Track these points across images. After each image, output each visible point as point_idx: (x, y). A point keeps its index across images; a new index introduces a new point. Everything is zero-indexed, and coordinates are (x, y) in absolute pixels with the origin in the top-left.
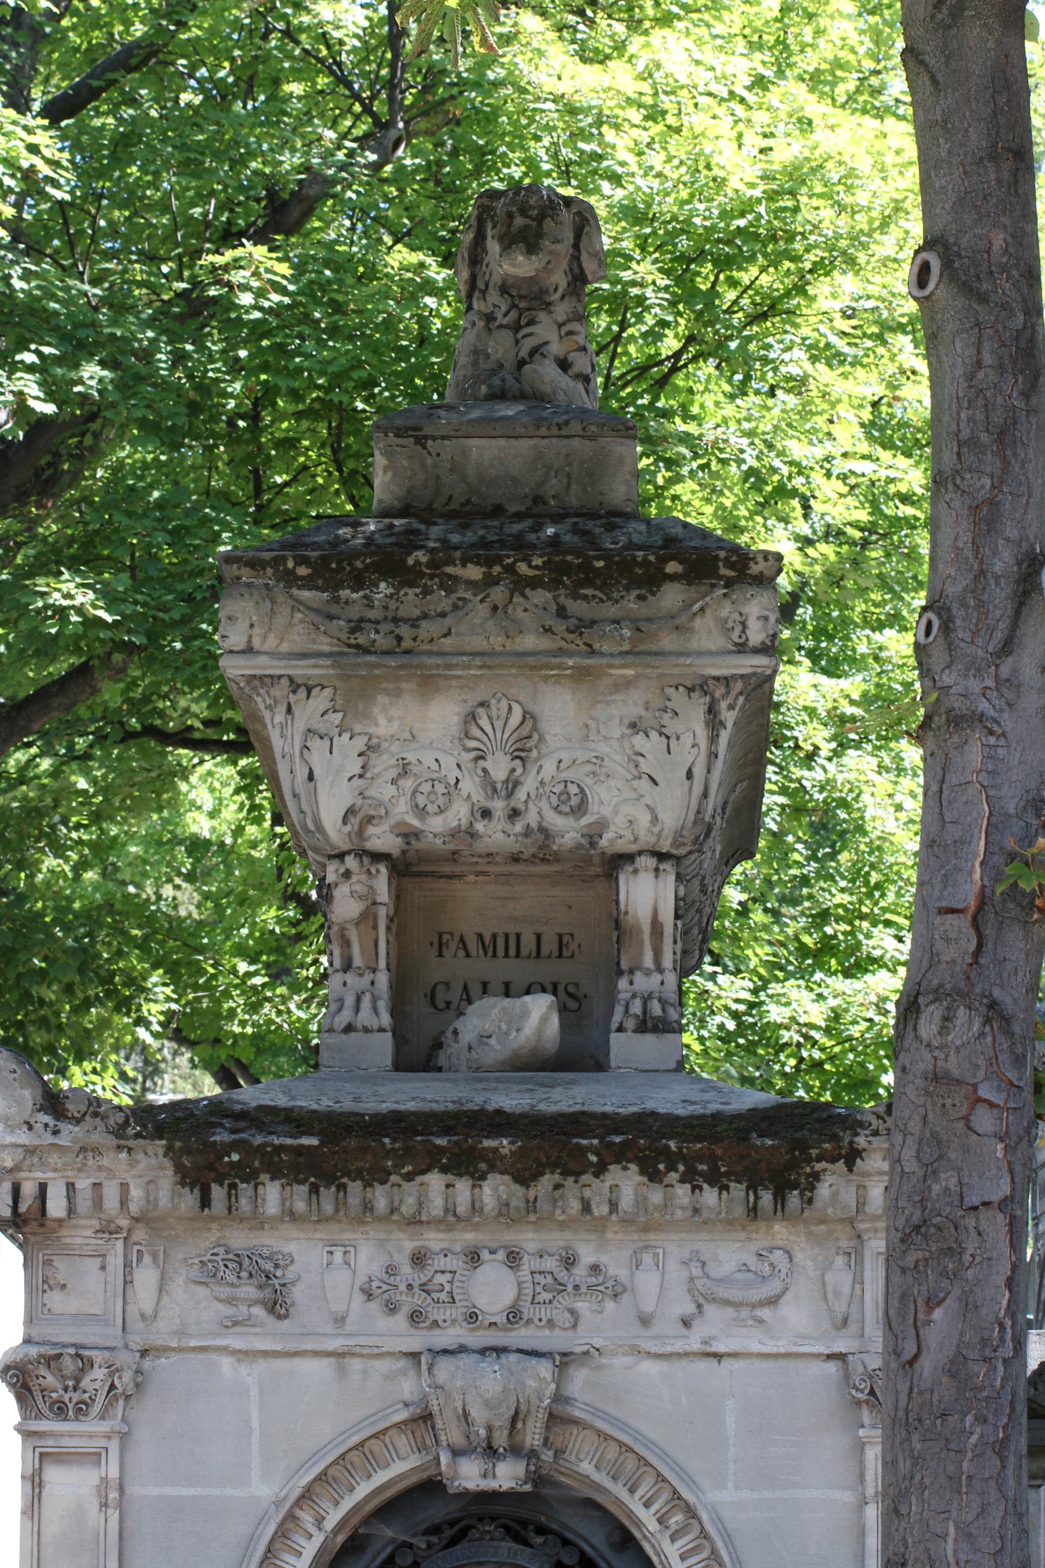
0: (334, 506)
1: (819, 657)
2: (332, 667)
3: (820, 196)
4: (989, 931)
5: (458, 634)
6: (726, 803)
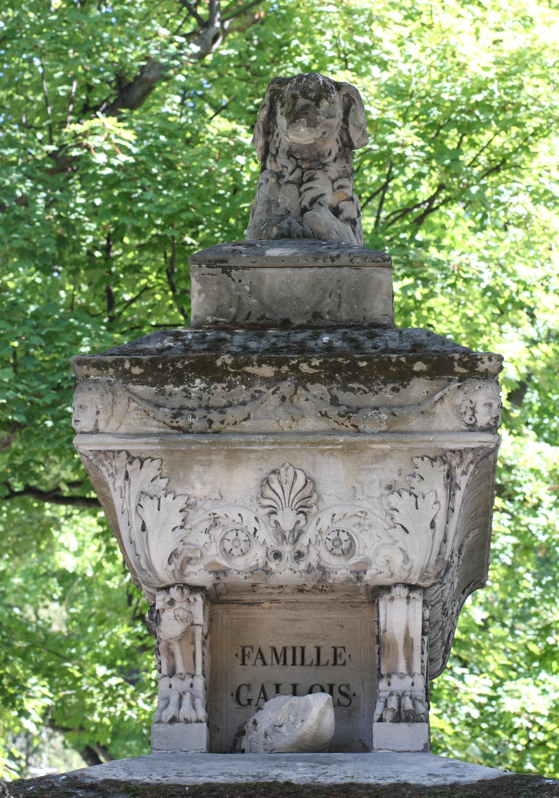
0: (168, 317)
1: (543, 430)
2: (159, 444)
3: (539, 76)
5: (255, 419)
6: (461, 546)
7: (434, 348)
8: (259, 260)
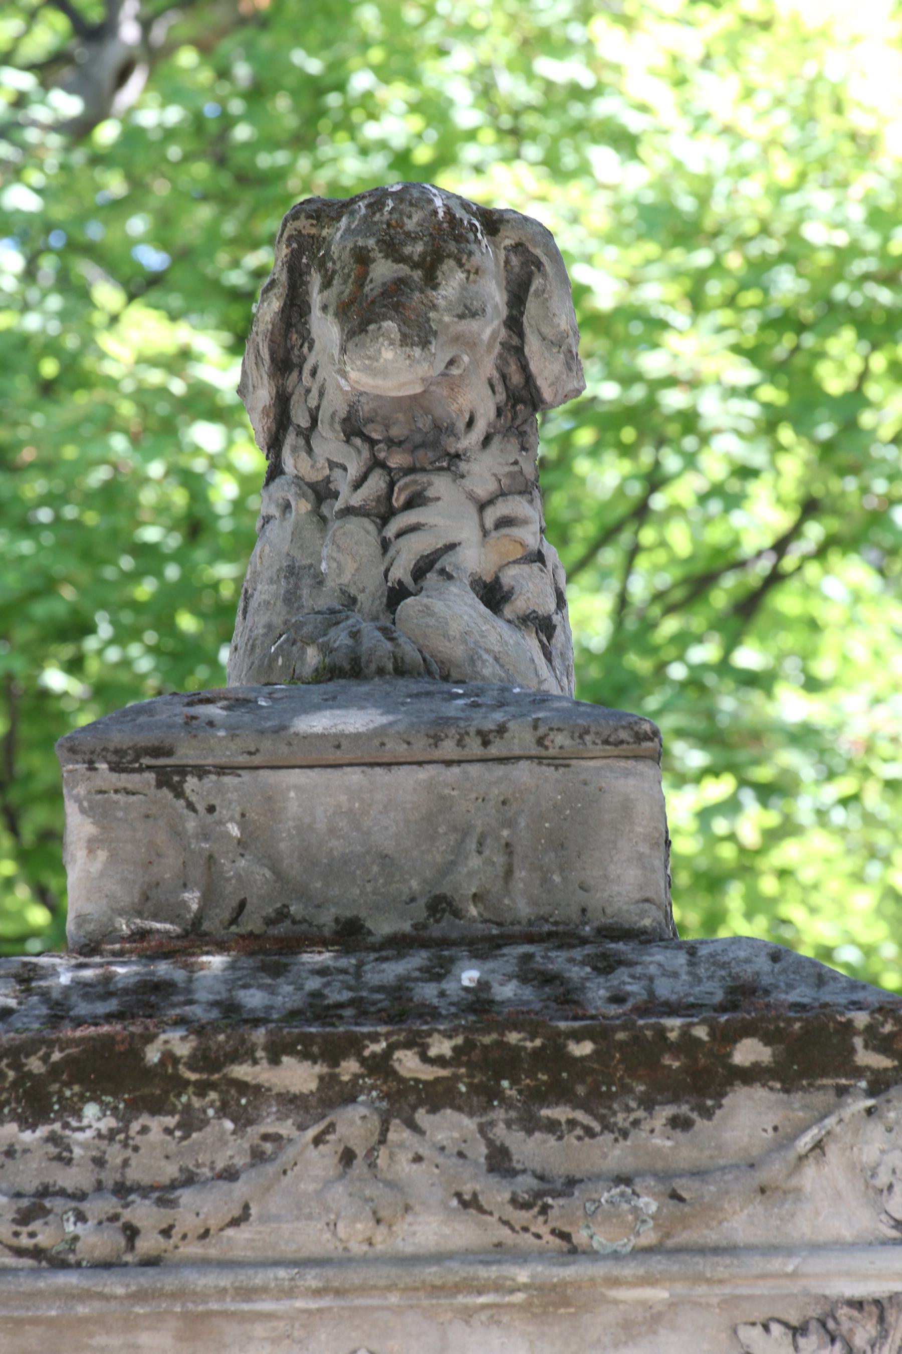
5: (265, 1219)
7: (793, 997)
8: (267, 744)
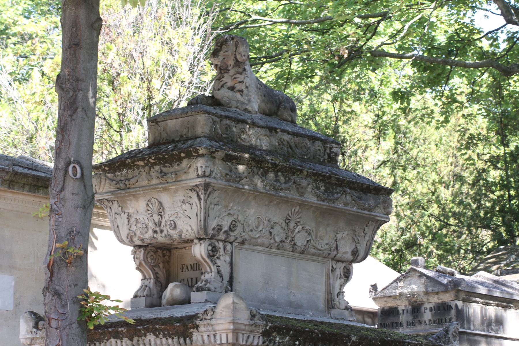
4: (55, 270)
